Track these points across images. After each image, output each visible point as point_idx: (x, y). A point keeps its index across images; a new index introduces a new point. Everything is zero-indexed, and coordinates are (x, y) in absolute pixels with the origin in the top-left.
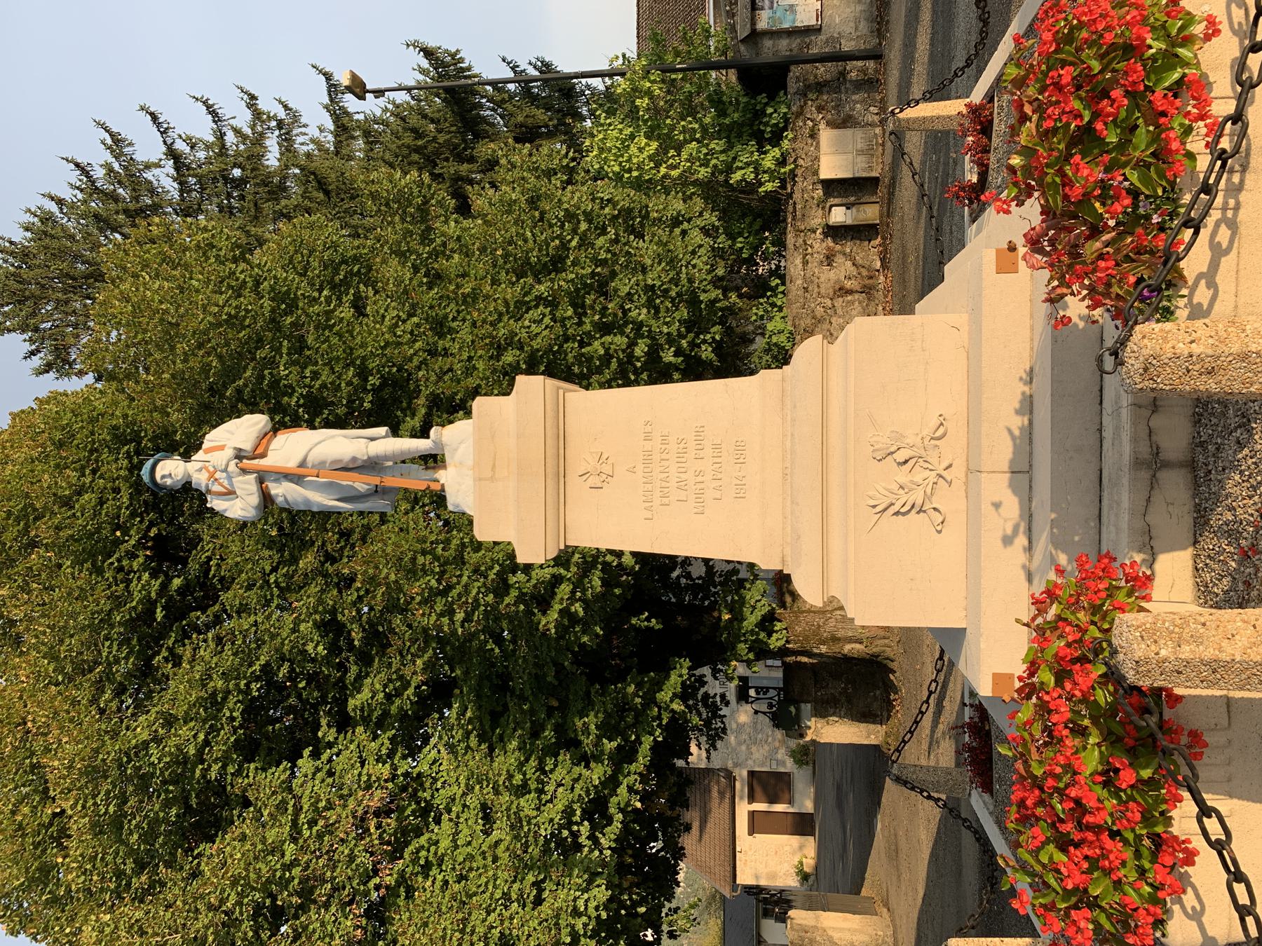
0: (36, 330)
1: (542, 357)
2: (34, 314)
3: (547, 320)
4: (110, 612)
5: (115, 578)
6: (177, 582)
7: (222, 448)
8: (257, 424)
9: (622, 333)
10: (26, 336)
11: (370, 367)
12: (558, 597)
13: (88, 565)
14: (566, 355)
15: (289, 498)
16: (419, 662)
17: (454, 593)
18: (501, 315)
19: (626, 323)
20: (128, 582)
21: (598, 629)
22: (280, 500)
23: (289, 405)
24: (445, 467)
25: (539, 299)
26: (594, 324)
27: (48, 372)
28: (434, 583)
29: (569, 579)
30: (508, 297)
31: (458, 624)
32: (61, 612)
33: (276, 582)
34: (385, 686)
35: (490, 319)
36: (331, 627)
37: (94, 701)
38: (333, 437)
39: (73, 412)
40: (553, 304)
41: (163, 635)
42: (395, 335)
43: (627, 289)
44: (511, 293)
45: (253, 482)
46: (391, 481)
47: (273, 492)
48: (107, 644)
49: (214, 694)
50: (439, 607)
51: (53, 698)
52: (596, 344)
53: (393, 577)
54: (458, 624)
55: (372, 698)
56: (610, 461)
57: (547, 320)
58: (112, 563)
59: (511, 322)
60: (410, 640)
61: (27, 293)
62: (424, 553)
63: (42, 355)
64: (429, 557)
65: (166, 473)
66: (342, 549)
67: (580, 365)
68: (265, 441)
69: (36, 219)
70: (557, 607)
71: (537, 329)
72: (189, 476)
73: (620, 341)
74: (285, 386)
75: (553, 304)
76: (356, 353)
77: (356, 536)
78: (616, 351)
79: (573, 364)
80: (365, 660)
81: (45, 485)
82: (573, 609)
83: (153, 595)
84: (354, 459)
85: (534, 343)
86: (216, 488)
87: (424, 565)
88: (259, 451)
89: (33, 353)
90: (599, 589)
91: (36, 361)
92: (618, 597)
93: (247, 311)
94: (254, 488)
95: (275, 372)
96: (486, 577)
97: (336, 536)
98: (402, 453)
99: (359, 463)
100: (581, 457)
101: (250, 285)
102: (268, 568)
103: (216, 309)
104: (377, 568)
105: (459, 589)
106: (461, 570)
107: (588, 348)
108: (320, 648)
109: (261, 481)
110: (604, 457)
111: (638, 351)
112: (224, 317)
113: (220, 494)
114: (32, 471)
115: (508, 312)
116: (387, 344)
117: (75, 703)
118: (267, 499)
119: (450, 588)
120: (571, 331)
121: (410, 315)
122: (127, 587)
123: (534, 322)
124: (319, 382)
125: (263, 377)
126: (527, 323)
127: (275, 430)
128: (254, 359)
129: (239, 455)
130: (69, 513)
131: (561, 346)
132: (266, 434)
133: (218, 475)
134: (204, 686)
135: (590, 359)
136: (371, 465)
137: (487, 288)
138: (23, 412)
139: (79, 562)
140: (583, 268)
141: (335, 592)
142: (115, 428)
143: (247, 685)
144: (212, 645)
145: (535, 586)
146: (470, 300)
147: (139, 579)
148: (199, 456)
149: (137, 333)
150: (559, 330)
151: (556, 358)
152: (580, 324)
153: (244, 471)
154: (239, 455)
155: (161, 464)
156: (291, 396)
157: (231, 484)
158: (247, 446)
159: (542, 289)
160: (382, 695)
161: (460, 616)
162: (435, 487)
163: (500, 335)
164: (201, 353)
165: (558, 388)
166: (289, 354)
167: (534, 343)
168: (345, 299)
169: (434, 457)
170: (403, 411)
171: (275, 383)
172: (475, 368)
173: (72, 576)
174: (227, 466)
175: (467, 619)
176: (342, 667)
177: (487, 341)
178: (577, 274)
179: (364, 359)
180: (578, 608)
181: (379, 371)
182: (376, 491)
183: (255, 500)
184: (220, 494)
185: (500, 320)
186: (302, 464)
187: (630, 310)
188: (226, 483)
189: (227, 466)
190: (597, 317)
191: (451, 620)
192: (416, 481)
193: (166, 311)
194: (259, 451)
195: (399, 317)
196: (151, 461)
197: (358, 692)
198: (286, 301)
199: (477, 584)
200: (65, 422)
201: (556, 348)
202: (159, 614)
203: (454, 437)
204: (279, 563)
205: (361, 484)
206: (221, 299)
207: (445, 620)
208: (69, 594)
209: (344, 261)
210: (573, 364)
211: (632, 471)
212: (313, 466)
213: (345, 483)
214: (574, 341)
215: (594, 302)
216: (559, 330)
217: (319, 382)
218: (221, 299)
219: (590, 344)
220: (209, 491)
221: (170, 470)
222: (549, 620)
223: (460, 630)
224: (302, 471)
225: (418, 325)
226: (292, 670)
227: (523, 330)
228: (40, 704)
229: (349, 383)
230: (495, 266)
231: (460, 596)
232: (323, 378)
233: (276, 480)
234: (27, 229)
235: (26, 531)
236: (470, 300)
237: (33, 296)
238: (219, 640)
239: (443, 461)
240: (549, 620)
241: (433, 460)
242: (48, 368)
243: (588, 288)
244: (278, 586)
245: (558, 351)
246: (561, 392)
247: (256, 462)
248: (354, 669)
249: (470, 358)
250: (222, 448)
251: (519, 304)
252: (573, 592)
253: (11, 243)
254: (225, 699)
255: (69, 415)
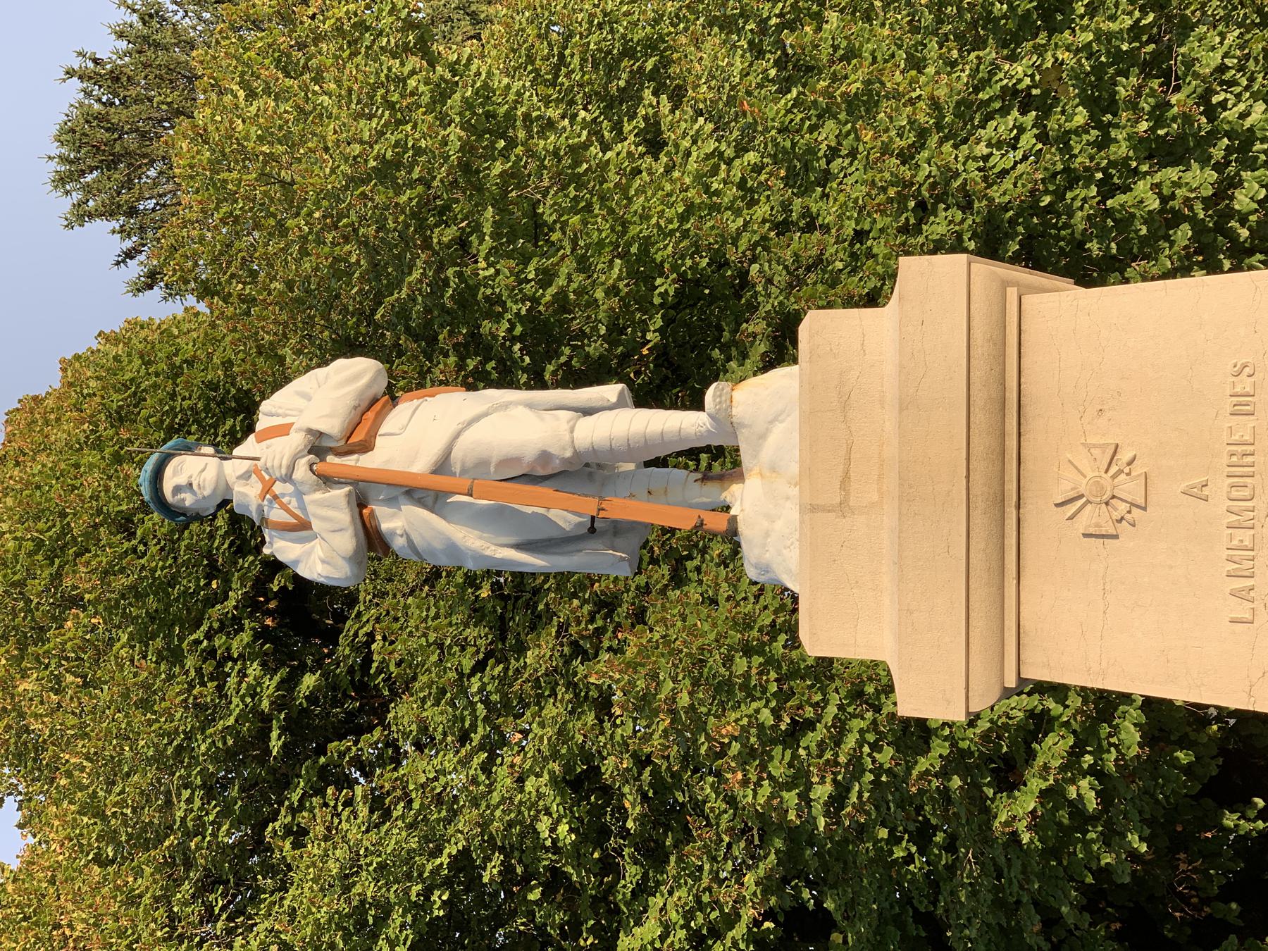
0: (132, 212)
1: (1013, 222)
2: (128, 184)
3: (1027, 140)
4: (189, 737)
5: (199, 671)
6: (309, 681)
7: (283, 430)
8: (356, 377)
9: (1205, 161)
10: (115, 225)
11: (658, 258)
12: (1040, 761)
13: (159, 643)
14: (1071, 215)
15: (417, 541)
16: (749, 879)
17: (811, 739)
18: (923, 134)
19: (1213, 136)
20: (220, 677)
21: (1133, 839)
22: (398, 543)
23: (495, 337)
24: (740, 478)
25: (1010, 94)
26: (1137, 142)
27: (150, 287)
28: (766, 716)
29: (1067, 724)
30: (941, 93)
31: (818, 809)
32: (108, 731)
33: (481, 690)
34: (689, 916)
35: (900, 143)
36: (582, 782)
37: (164, 899)
38: (506, 406)
39: (142, 357)
40: (1036, 101)
41: (284, 784)
42: (707, 189)
43: (1216, 58)
44: (948, 87)
45: (343, 503)
46: (621, 508)
47: (385, 526)
48: (186, 794)
49: (361, 908)
50: (778, 769)
51: (96, 889)
52: (1142, 187)
53: (684, 699)
54: (818, 809)
55: (663, 938)
56: (1138, 469)
57: (1027, 140)
58: (198, 642)
59: (947, 147)
60: (730, 830)
61: (118, 148)
62: (748, 651)
63: (142, 257)
64: (757, 660)
65: (182, 480)
66: (599, 632)
67: (1103, 236)
68: (370, 415)
69: (135, 17)
70: (1036, 784)
71: (1007, 159)
72: (228, 488)
73: (1201, 178)
74: (487, 298)
75: (1036, 101)
76: (633, 230)
77: (623, 610)
78: (1187, 201)
79: (1086, 237)
80: (654, 856)
81: (88, 494)
82: (1072, 792)
83: (265, 705)
84: (545, 456)
85: (995, 192)
86: (276, 515)
87: (747, 676)
88: (358, 437)
89: (129, 255)
90: (1134, 751)
91: (135, 269)
92: (1188, 770)
93: (418, 151)
94: (344, 516)
95: (468, 271)
96: (877, 709)
97: (587, 608)
98: (647, 443)
99: (556, 467)
100: (1062, 459)
101: (426, 99)
102: (467, 664)
103: (357, 149)
104: (654, 676)
105: (820, 733)
106: (823, 691)
107: (1121, 198)
108: (563, 829)
109: (360, 503)
110: (1124, 456)
111: (1242, 200)
112: (372, 164)
113: (285, 528)
114: (77, 466)
115: (939, 127)
116: (690, 209)
117: (133, 900)
118: (373, 541)
119: (800, 727)
120: (1080, 161)
121: (741, 150)
122: (220, 688)
123: (999, 144)
124: (552, 290)
125: (446, 283)
126: (982, 149)
127: (392, 396)
128: (427, 244)
129: (318, 446)
130: (126, 545)
131: (1059, 195)
132: (375, 401)
133: (278, 488)
134: (347, 889)
135: (1124, 222)
136: (584, 471)
137: (896, 78)
138: (77, 357)
139: (143, 637)
140: (1113, 18)
141: (590, 719)
142: (213, 386)
143: (427, 893)
144: (363, 811)
145: (985, 736)
146: (863, 105)
147: (242, 675)
148: (249, 446)
149: (219, 202)
150: (1054, 160)
151: (1046, 224)
152: (1104, 142)
153: (327, 481)
154: (318, 446)
155: (175, 461)
156: (498, 317)
157: (303, 507)
158: (332, 425)
159: (1019, 71)
160: (682, 934)
161: (822, 792)
162: (717, 523)
163: (920, 178)
164: (329, 237)
165: (1005, 284)
166: (496, 235)
167: (995, 192)
168: (627, 128)
169: (717, 453)
170: (725, 348)
171: (467, 297)
172: (870, 255)
173: (128, 663)
174: (292, 467)
175: (837, 801)
176: (609, 867)
177: (892, 192)
178: (1098, 34)
179: (646, 243)
180: (1085, 791)
181: (675, 268)
182: (592, 530)
183: (346, 541)
184: (285, 528)
185: (920, 144)
186: (442, 466)
187: (1223, 105)
188: (293, 505)
189: (292, 467)
190: (1144, 126)
191: (805, 798)
192: (676, 506)
193: (271, 157)
194: (358, 437)
195: (721, 154)
196: (154, 458)
197: (639, 923)
198: (489, 125)
199: (857, 724)
200: (128, 376)
201: (1047, 200)
202: (276, 743)
203: (755, 403)
204: (489, 655)
205: (564, 514)
206: (366, 128)
207: (791, 798)
208: (126, 695)
209: (628, 52)
210: (1086, 237)
211: (1198, 493)
212: (464, 471)
213: (529, 510)
214: (1089, 181)
215: (1138, 91)
216: (1054, 160)
217: (552, 290)
218: (366, 128)
219: (1126, 189)
220: (264, 520)
221: (194, 474)
222: (1017, 810)
223: (822, 822)
224: (441, 482)
225: (757, 169)
226: (507, 869)
227: (972, 165)
228: (77, 899)
229: (612, 291)
230: (915, 30)
231: (821, 746)
232: (561, 281)
233: (391, 501)
234: (121, 35)
235: (57, 577)
236: (863, 105)
237: (128, 154)
238: (377, 803)
239: (736, 463)
240: (1017, 810)
241: (716, 460)
242: (152, 279)
243: (1123, 62)
244: (486, 702)
245: (1050, 209)
246: (1012, 293)
247: (350, 460)
248: (632, 873)
249: (860, 235)
250: (283, 430)
251: (965, 108)
252: (1075, 753)
253: (96, 61)
254: (383, 920)
255: (137, 362)
